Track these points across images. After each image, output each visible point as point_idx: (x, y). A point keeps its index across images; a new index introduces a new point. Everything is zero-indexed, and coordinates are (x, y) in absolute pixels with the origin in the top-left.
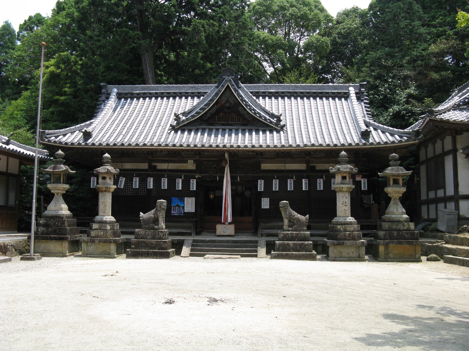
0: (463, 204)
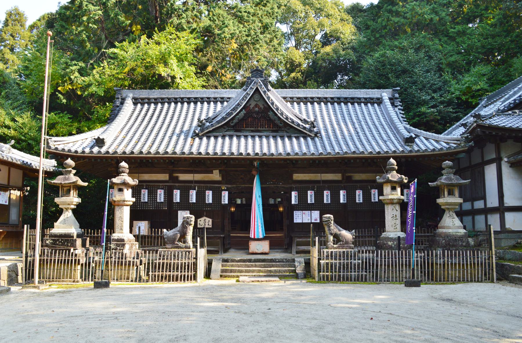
0: (509, 217)
